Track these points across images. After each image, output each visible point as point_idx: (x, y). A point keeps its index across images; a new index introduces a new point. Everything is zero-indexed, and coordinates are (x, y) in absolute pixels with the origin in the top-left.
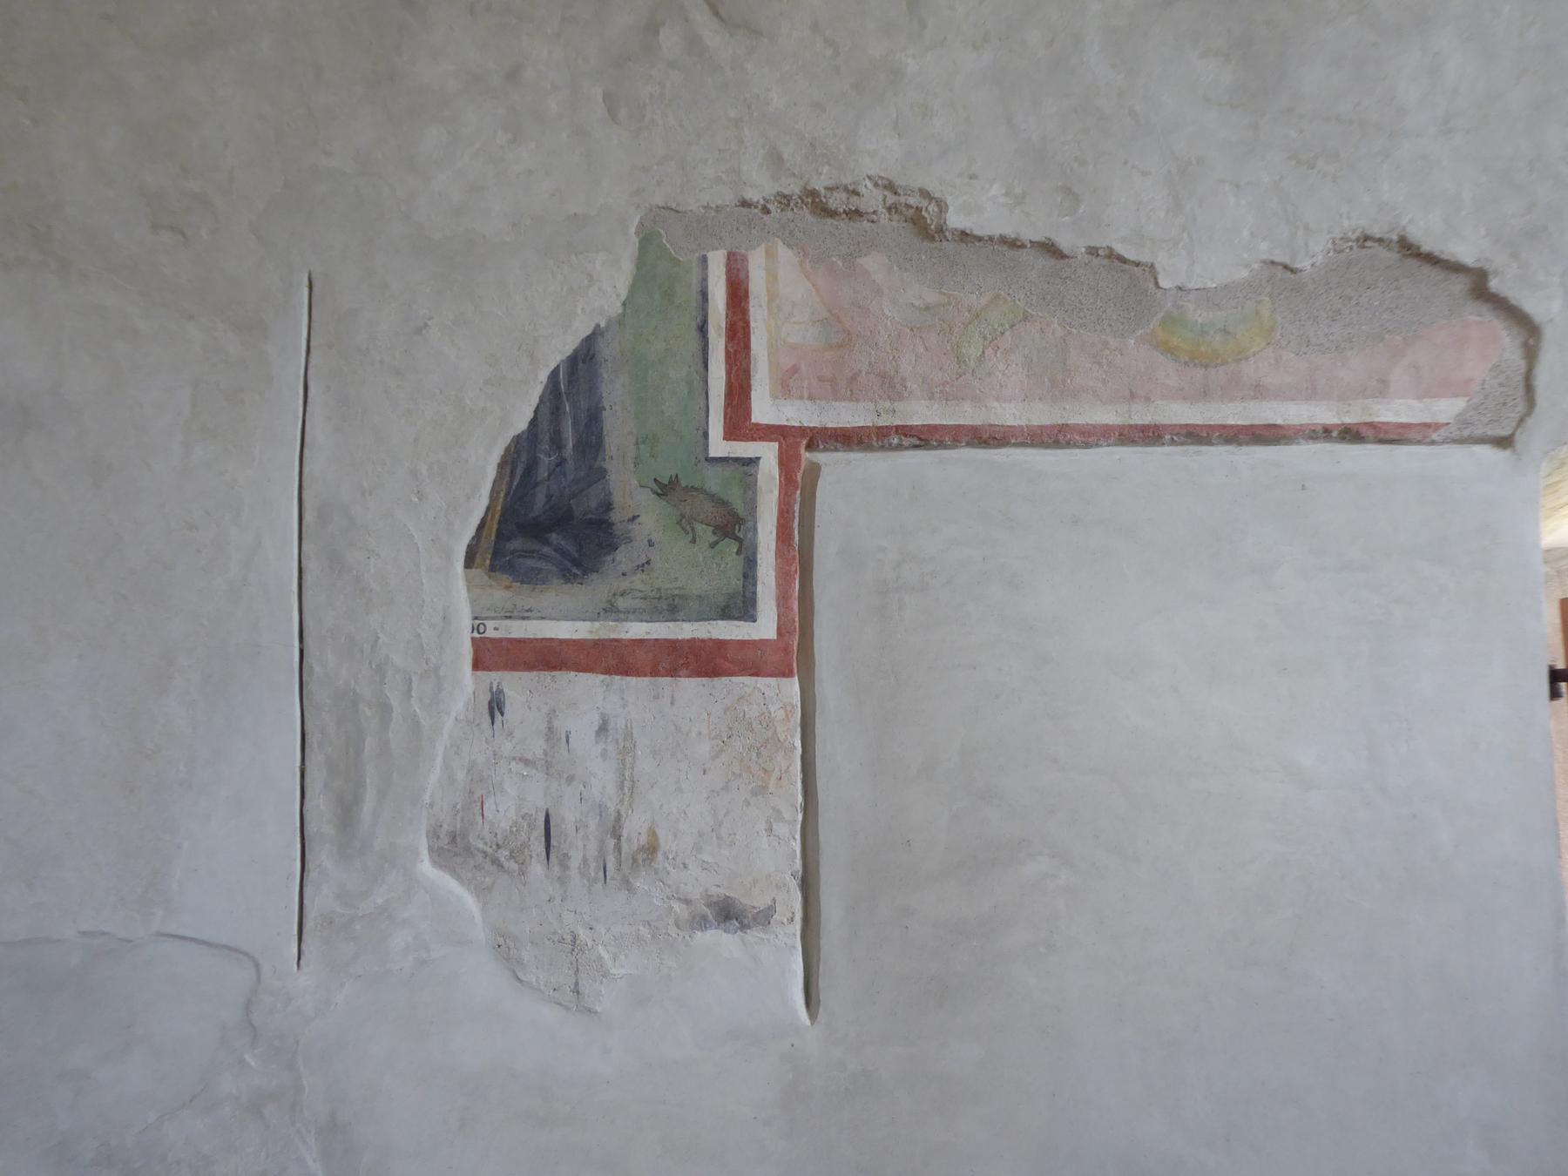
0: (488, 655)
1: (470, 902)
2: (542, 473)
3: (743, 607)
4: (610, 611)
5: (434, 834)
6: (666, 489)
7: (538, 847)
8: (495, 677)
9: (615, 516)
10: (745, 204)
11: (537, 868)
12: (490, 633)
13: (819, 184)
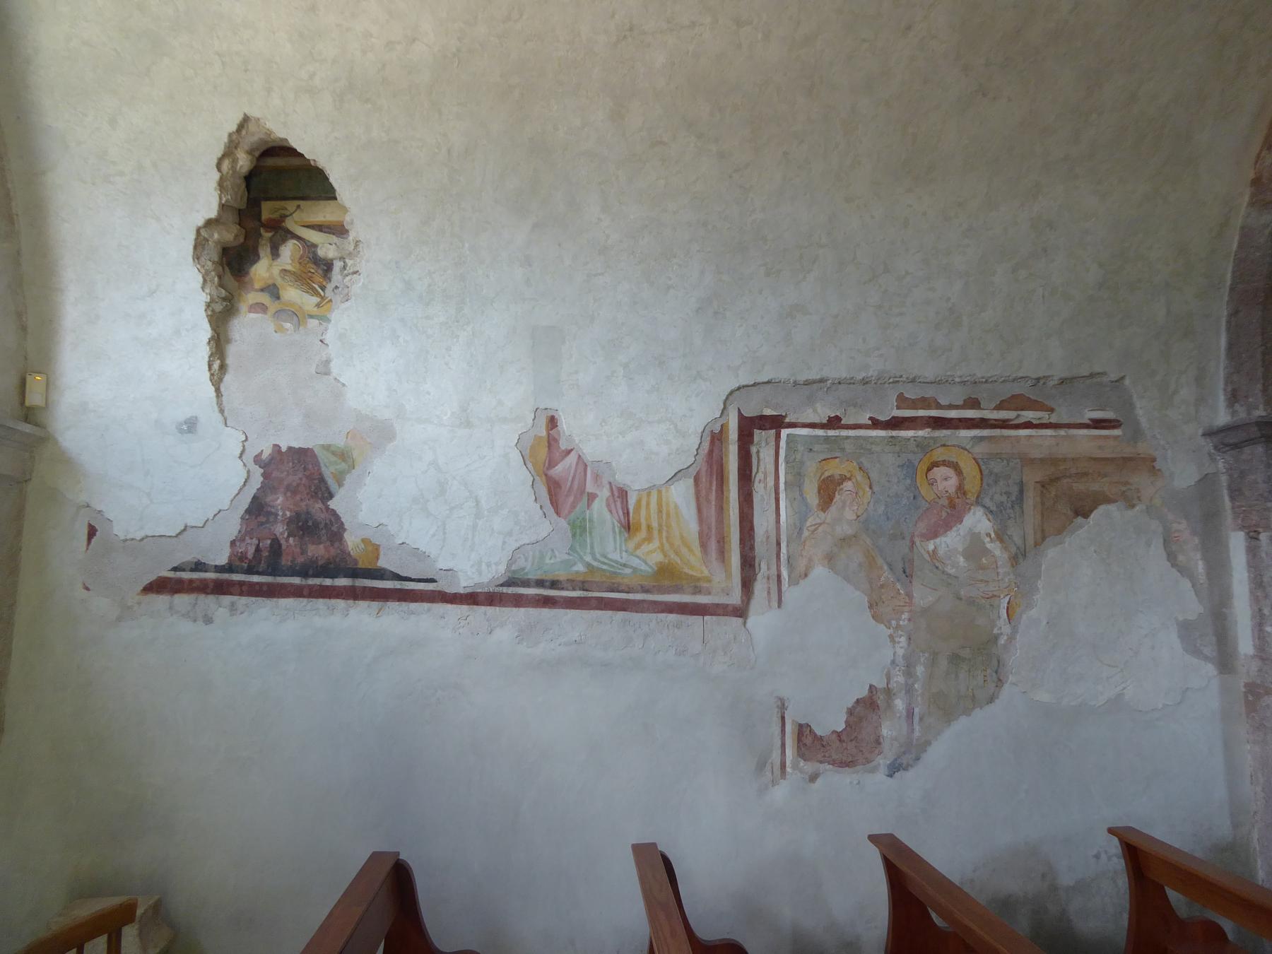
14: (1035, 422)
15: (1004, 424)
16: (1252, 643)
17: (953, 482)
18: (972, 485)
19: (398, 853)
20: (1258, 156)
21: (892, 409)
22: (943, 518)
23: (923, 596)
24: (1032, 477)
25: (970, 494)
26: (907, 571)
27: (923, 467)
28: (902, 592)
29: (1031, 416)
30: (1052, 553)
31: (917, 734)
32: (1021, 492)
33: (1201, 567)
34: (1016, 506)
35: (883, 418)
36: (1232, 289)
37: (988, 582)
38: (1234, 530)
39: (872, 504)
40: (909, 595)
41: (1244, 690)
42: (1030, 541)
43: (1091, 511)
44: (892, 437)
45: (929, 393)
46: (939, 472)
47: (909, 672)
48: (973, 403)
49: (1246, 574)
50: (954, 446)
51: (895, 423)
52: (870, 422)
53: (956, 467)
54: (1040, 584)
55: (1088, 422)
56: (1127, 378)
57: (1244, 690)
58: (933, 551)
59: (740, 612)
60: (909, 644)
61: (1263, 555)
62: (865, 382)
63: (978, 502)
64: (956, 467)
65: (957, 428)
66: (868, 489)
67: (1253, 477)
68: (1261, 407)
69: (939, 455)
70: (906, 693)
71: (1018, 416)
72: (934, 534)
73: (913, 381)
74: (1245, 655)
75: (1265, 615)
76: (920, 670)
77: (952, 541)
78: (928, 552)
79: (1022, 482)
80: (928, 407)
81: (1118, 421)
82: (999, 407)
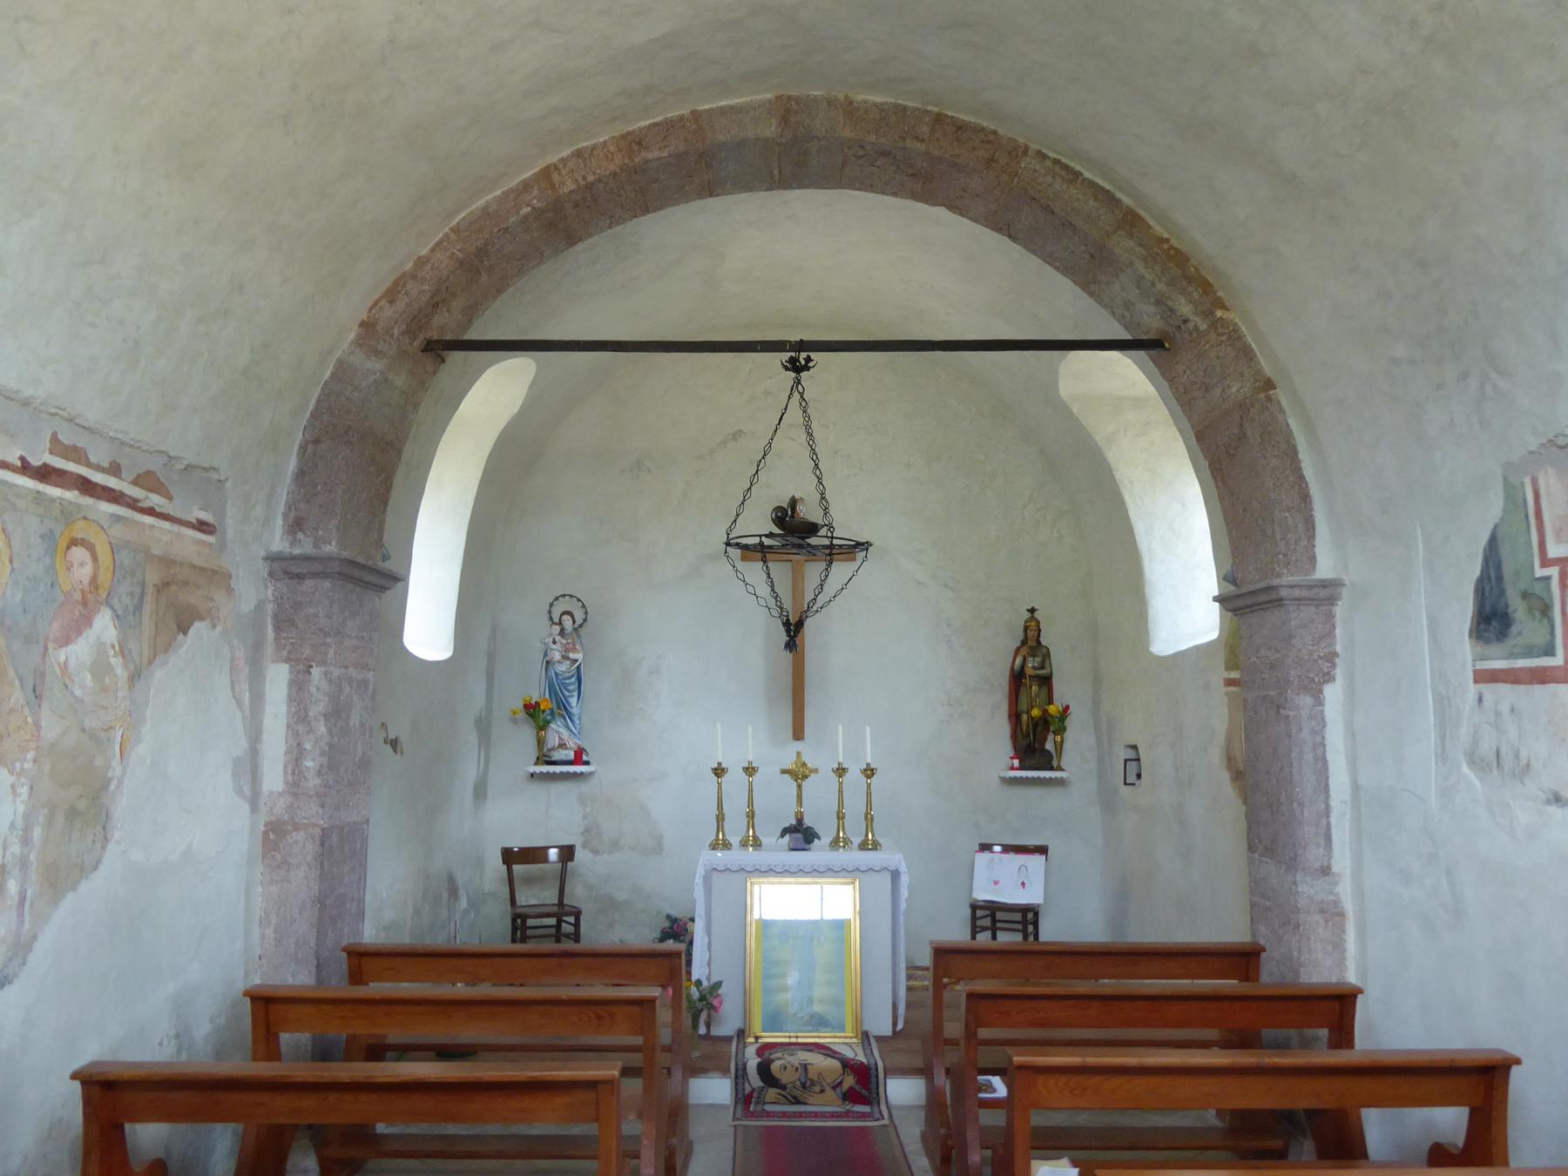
0: (1484, 677)
1: (1477, 782)
2: (1487, 594)
3: (1549, 651)
4: (1512, 656)
5: (1465, 754)
6: (1525, 595)
7: (1495, 763)
8: (1481, 686)
9: (1510, 611)
10: (1531, 453)
11: (1495, 772)
12: (1478, 668)
13: (1551, 437)
14: (158, 509)
15: (133, 504)
16: (282, 779)
17: (87, 570)
18: (105, 579)
19: (1264, 950)
20: (376, 303)
21: (44, 452)
22: (75, 618)
23: (51, 727)
24: (153, 576)
25: (102, 589)
26: (38, 689)
27: (63, 544)
28: (29, 720)
29: (157, 502)
30: (159, 675)
31: (27, 926)
32: (143, 594)
33: (247, 696)
34: (137, 612)
35: (35, 462)
36: (313, 416)
37: (107, 708)
38: (275, 661)
39: (9, 586)
40: (37, 725)
41: (263, 829)
42: (145, 660)
43: (189, 627)
44: (38, 492)
45: (81, 441)
46: (79, 553)
47: (26, 841)
48: (115, 470)
49: (284, 708)
50: (94, 521)
51: (45, 474)
52: (19, 463)
53: (90, 548)
54: (148, 712)
55: (194, 521)
56: (230, 480)
57: (263, 829)
58: (65, 663)
59: (1125, 784)
60: (30, 796)
61: (314, 690)
62: (26, 403)
63: (108, 603)
64: (90, 548)
65: (98, 497)
66: (7, 562)
67: (311, 611)
68: (334, 543)
69: (80, 530)
70: (20, 869)
71: (147, 497)
72: (65, 641)
73: (71, 420)
74: (271, 793)
75: (305, 749)
76: (37, 832)
77: (79, 652)
78: (59, 664)
79: (144, 581)
80: (77, 461)
81: (213, 526)
82: (135, 483)
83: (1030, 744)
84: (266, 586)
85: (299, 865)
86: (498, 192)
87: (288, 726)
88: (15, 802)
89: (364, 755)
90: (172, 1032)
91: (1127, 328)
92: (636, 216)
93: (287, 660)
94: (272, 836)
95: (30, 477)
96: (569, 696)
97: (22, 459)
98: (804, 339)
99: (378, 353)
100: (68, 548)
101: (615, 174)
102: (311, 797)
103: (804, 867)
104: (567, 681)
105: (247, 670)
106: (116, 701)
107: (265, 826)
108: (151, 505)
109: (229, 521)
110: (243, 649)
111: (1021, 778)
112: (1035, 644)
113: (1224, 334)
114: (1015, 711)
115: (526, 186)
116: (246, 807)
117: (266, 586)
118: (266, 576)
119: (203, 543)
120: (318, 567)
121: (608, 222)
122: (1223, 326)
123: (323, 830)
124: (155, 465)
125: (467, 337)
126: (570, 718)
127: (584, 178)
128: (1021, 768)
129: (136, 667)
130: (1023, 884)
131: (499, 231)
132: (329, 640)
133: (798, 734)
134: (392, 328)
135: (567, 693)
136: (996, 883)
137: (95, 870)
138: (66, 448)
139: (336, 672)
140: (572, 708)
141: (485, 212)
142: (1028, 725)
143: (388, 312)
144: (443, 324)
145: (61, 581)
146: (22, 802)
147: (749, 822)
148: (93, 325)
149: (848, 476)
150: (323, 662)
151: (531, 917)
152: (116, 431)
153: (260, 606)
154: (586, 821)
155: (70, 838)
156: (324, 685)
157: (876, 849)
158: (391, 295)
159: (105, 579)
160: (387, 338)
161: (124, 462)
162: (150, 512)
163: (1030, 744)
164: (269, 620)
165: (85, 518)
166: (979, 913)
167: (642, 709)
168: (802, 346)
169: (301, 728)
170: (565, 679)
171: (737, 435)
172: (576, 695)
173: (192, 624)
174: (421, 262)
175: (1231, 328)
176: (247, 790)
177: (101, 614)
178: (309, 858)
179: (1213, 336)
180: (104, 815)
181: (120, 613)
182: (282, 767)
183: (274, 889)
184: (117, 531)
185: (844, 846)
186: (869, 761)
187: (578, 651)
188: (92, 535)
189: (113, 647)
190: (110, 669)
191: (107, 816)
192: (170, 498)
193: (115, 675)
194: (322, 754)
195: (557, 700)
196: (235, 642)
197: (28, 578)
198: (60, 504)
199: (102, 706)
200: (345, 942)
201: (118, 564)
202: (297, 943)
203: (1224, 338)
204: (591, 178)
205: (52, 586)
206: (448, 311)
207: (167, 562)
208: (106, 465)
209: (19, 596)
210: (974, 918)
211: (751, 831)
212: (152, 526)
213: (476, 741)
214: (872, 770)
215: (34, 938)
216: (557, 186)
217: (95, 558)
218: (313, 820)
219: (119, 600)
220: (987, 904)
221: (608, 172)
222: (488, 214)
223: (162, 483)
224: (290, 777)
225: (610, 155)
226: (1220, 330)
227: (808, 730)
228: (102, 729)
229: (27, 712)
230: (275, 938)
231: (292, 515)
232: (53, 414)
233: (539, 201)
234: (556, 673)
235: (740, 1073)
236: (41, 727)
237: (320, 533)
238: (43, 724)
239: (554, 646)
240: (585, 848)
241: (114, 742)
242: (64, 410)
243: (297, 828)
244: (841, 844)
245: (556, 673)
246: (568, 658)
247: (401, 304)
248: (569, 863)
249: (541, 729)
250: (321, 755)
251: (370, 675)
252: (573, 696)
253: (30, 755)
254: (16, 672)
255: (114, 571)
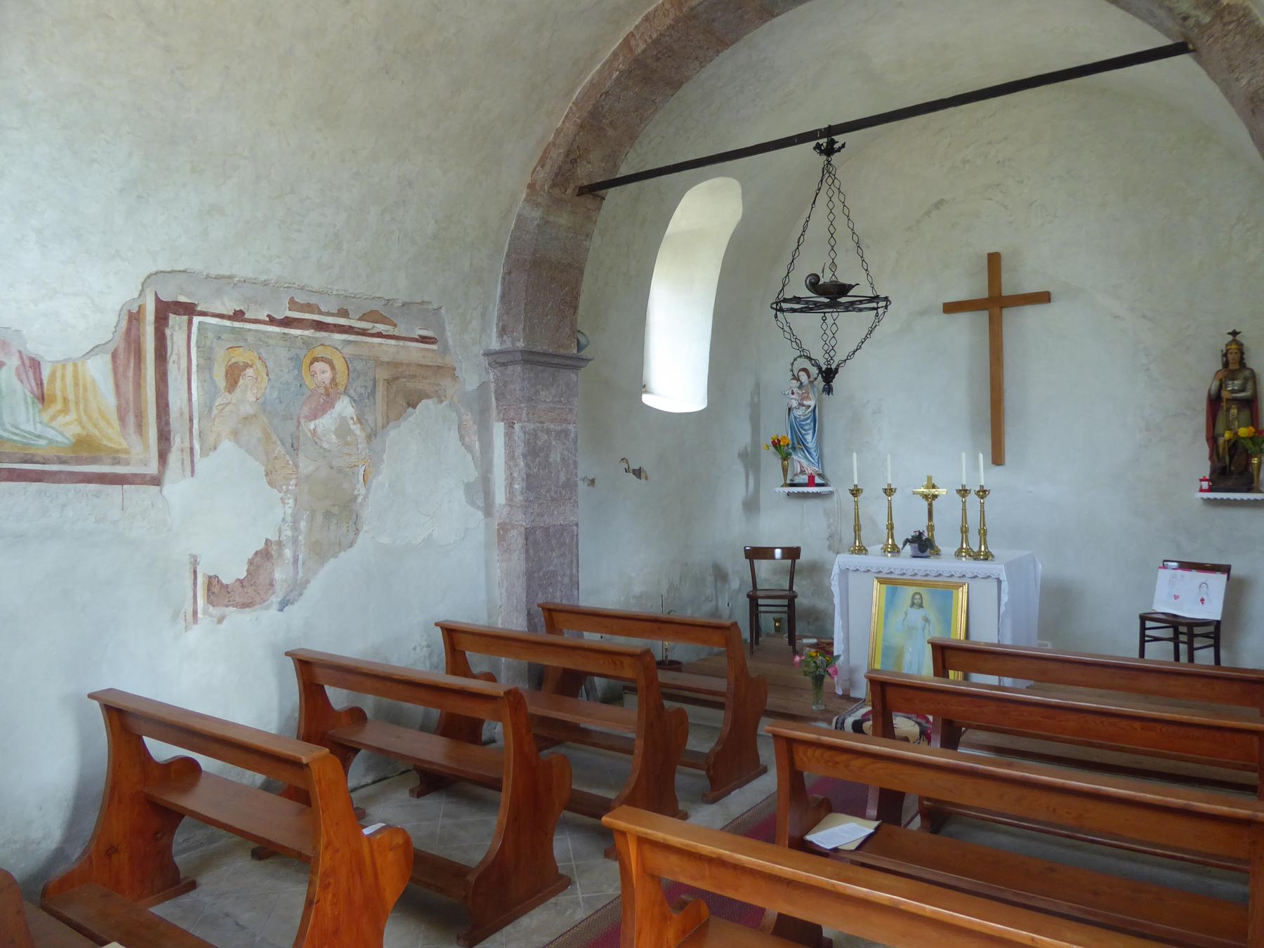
15: (363, 333)
17: (328, 375)
21: (285, 310)
23: (306, 466)
24: (382, 375)
28: (290, 462)
30: (393, 434)
31: (301, 575)
32: (374, 386)
35: (279, 316)
36: (507, 256)
38: (497, 421)
40: (296, 466)
41: (497, 527)
42: (380, 424)
43: (418, 404)
44: (284, 334)
45: (313, 301)
46: (319, 366)
47: (295, 528)
48: (344, 313)
50: (329, 346)
51: (287, 322)
52: (268, 319)
53: (330, 363)
54: (385, 457)
58: (314, 430)
62: (265, 284)
63: (346, 392)
64: (330, 363)
65: (332, 331)
68: (522, 340)
69: (319, 352)
72: (314, 416)
77: (326, 423)
78: (310, 430)
79: (375, 378)
80: (312, 312)
82: (361, 319)
83: (1225, 467)
84: (488, 373)
85: (515, 551)
86: (598, 66)
87: (506, 463)
88: (284, 507)
89: (569, 480)
90: (424, 644)
91: (1169, 37)
92: (718, 52)
93: (503, 420)
94: (501, 532)
95: (277, 326)
96: (805, 434)
97: (268, 316)
98: (832, 125)
99: (538, 205)
100: (312, 363)
101: (671, 27)
102: (519, 507)
103: (894, 569)
104: (804, 423)
105: (476, 428)
106: (358, 450)
107: (498, 525)
108: (379, 331)
109: (448, 334)
110: (470, 414)
111: (1222, 499)
112: (1237, 367)
113: (1233, 21)
114: (1211, 435)
115: (615, 54)
116: (480, 515)
117: (488, 373)
118: (487, 366)
119: (428, 350)
120: (510, 358)
121: (595, 82)
122: (1229, 13)
123: (526, 529)
124: (374, 306)
125: (618, 176)
126: (807, 450)
127: (651, 37)
128: (1210, 490)
129: (372, 430)
130: (1202, 600)
131: (601, 96)
132: (523, 405)
133: (997, 458)
134: (544, 185)
135: (803, 432)
136: (1176, 597)
137: (351, 546)
138: (302, 305)
139: (531, 426)
140: (807, 443)
141: (593, 85)
142: (1224, 448)
143: (542, 174)
144: (589, 171)
145: (307, 384)
146: (290, 507)
147: (888, 533)
148: (299, 231)
149: (1043, 224)
150: (520, 420)
151: (762, 598)
152: (337, 290)
153: (483, 386)
154: (830, 530)
155: (329, 528)
156: (522, 435)
157: (987, 559)
158: (542, 163)
159: (342, 378)
160: (542, 193)
161: (350, 308)
162: (379, 335)
163: (1225, 467)
164: (493, 395)
165: (322, 345)
166: (1149, 624)
167: (868, 442)
168: (831, 131)
169: (511, 463)
170: (802, 421)
171: (939, 205)
172: (811, 434)
173: (420, 401)
174: (558, 132)
175: (1240, 14)
176: (480, 503)
177: (341, 401)
178: (520, 546)
179: (1218, 27)
180: (354, 516)
181: (356, 398)
182: (504, 488)
183: (504, 565)
184: (348, 350)
185: (965, 556)
186: (982, 484)
187: (810, 399)
188: (328, 354)
189: (352, 419)
190: (350, 432)
191: (357, 516)
192: (395, 325)
193: (355, 435)
194: (523, 480)
195: (797, 438)
196: (462, 410)
197: (281, 383)
198: (302, 338)
199: (347, 454)
200: (540, 601)
201: (351, 369)
202: (517, 599)
203: (1231, 26)
204: (654, 36)
205: (301, 386)
206: (589, 163)
207: (394, 364)
208: (336, 312)
209: (275, 394)
210: (1143, 628)
211: (890, 540)
212: (381, 344)
213: (742, 470)
214: (985, 491)
215: (308, 582)
216: (634, 49)
217: (333, 367)
218: (520, 523)
219: (355, 390)
220: (1171, 619)
221: (666, 27)
222: (594, 84)
223: (385, 317)
224: (508, 495)
225: (667, 12)
226: (1227, 19)
227: (1008, 456)
228: (348, 467)
229: (288, 458)
230: (507, 596)
231: (501, 324)
232: (288, 287)
233: (623, 65)
234: (795, 417)
235: (839, 725)
236: (299, 467)
237: (515, 334)
238: (300, 465)
239: (793, 396)
240: (830, 550)
241: (358, 474)
242: (294, 284)
243: (513, 527)
244: (964, 554)
245: (795, 417)
246: (803, 405)
247: (548, 167)
248: (797, 561)
249: (784, 460)
250: (522, 481)
251: (571, 427)
252: (808, 434)
253: (293, 482)
254: (278, 436)
255: (349, 374)
